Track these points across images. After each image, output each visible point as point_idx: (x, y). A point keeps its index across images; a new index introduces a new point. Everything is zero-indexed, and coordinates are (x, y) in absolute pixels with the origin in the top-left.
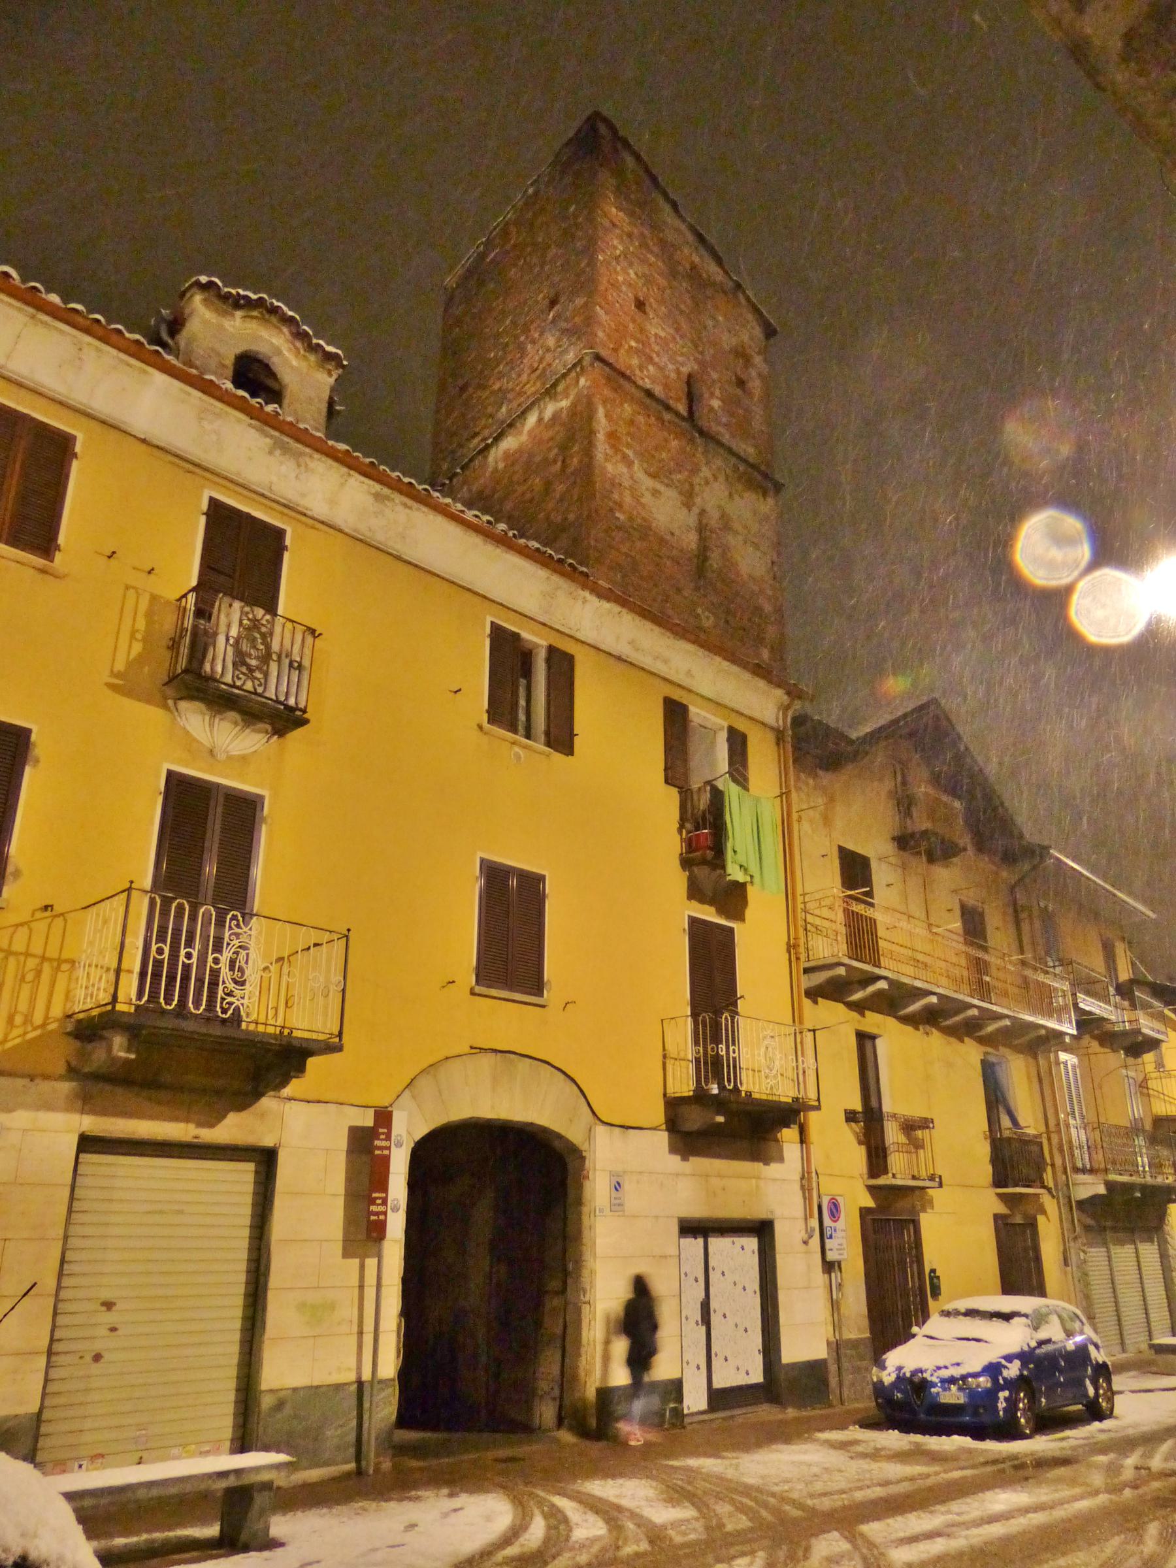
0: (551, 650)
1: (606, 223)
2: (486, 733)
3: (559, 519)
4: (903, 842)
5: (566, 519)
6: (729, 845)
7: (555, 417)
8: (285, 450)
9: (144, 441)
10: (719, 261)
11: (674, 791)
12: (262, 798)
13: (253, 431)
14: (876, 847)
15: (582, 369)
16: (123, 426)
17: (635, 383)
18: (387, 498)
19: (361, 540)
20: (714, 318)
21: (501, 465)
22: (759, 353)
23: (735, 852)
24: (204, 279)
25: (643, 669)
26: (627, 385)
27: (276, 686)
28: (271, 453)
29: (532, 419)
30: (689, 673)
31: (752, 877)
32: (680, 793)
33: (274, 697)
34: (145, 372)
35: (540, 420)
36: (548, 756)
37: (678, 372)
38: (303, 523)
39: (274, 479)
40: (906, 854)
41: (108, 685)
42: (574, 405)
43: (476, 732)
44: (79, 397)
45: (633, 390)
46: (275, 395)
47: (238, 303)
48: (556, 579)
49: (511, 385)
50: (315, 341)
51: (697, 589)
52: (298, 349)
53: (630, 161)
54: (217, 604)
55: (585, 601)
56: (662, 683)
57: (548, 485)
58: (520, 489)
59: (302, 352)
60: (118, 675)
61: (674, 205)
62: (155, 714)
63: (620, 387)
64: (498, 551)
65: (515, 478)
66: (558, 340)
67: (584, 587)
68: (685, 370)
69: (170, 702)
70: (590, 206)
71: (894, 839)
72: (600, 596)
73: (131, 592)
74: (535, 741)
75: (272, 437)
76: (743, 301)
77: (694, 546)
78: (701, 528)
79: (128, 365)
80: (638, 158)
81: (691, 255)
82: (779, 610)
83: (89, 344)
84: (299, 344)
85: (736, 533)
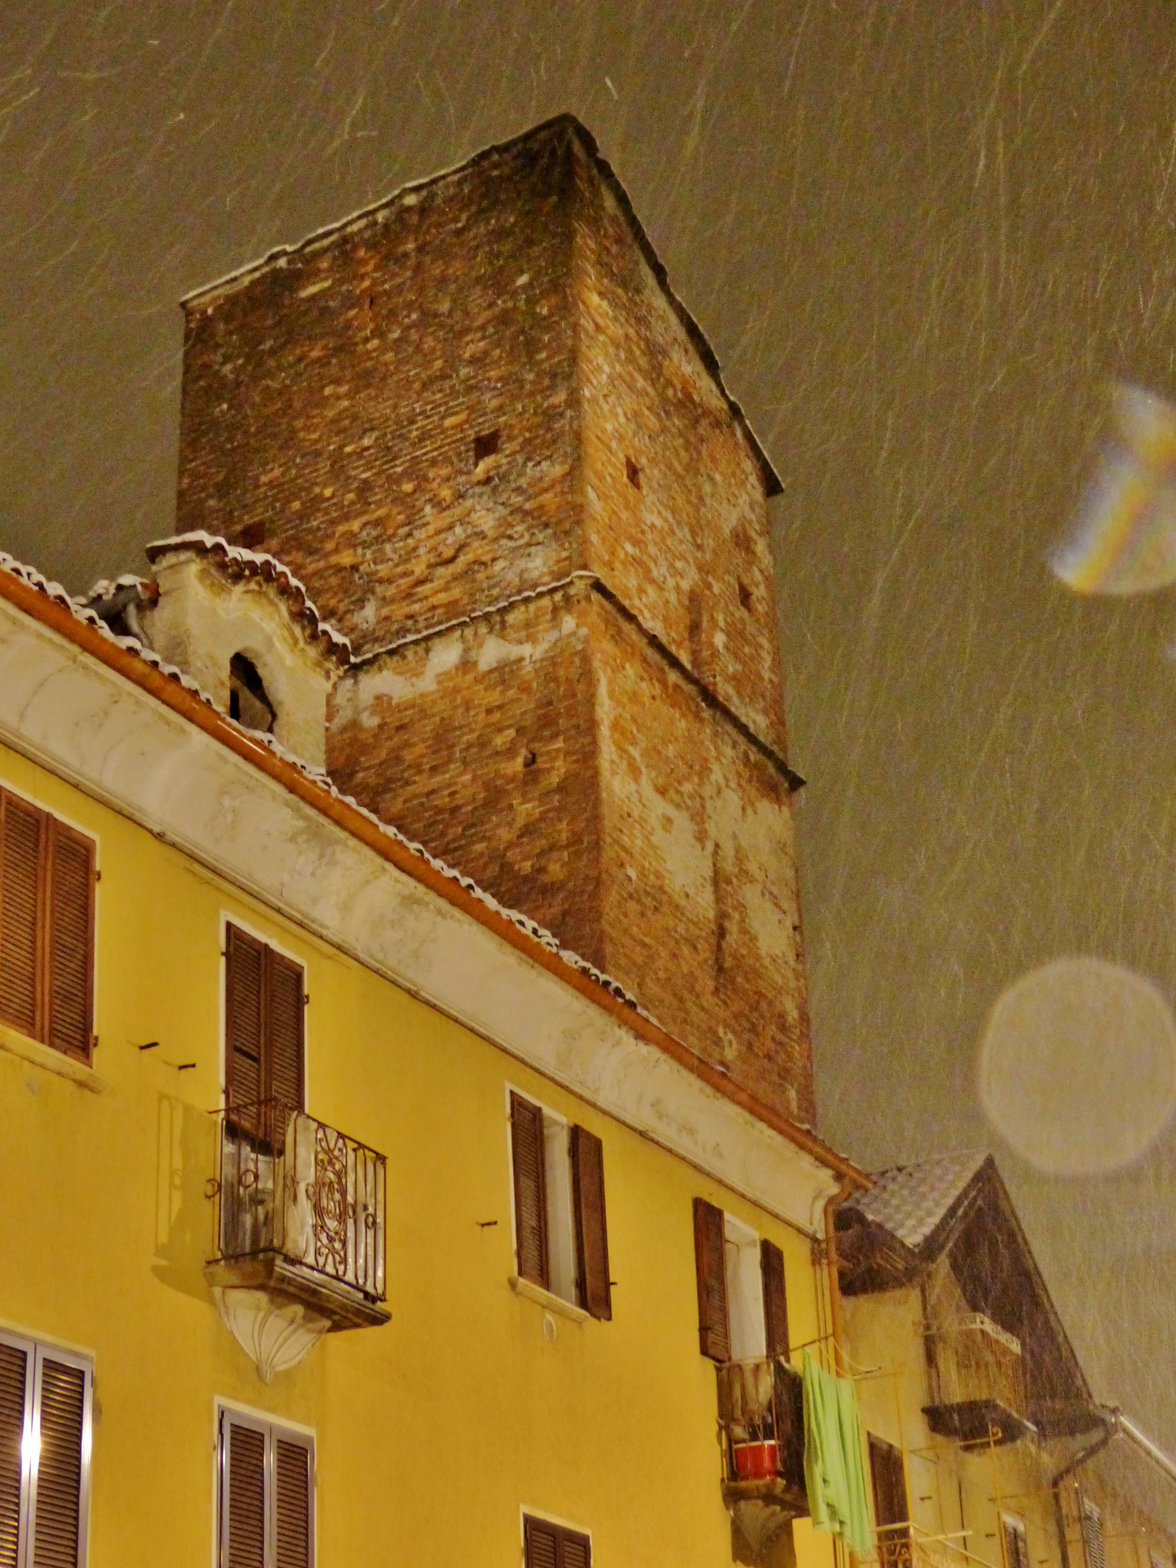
0: (576, 1132)
1: (590, 327)
2: (518, 1294)
3: (527, 866)
4: (937, 1418)
5: (541, 870)
6: (818, 1471)
7: (505, 673)
8: (314, 834)
9: (160, 837)
10: (711, 366)
11: (711, 1363)
12: (310, 1440)
13: (287, 810)
14: (909, 1435)
15: (567, 598)
16: (138, 816)
17: (639, 625)
18: (419, 902)
19: (377, 972)
20: (711, 479)
21: (370, 721)
22: (761, 534)
23: (825, 1481)
24: (209, 540)
25: (670, 1151)
26: (627, 627)
27: (359, 1264)
28: (293, 839)
29: (446, 655)
30: (717, 1151)
31: (842, 1523)
32: (718, 1370)
33: (354, 1282)
34: (183, 731)
35: (466, 665)
36: (580, 1323)
37: (678, 588)
38: (320, 952)
39: (286, 877)
40: (939, 1438)
41: (155, 1269)
42: (552, 660)
43: (506, 1292)
44: (110, 778)
45: (635, 637)
46: (270, 716)
47: (238, 573)
48: (593, 1011)
49: (383, 570)
50: (322, 626)
51: (716, 992)
52: (296, 641)
53: (609, 203)
54: (290, 1130)
55: (618, 1043)
56: (690, 1171)
57: (495, 797)
58: (423, 783)
59: (301, 644)
60: (161, 1251)
61: (659, 271)
62: (194, 1308)
63: (620, 631)
64: (533, 973)
65: (409, 756)
66: (504, 523)
67: (623, 1022)
68: (685, 585)
69: (217, 1290)
70: (559, 284)
71: (925, 1411)
72: (640, 1036)
73: (165, 1103)
74: (559, 1294)
75: (306, 818)
76: (739, 433)
77: (711, 914)
78: (718, 880)
79: (168, 723)
80: (622, 199)
81: (685, 365)
82: (804, 1018)
83: (129, 694)
84: (298, 631)
85: (752, 881)
